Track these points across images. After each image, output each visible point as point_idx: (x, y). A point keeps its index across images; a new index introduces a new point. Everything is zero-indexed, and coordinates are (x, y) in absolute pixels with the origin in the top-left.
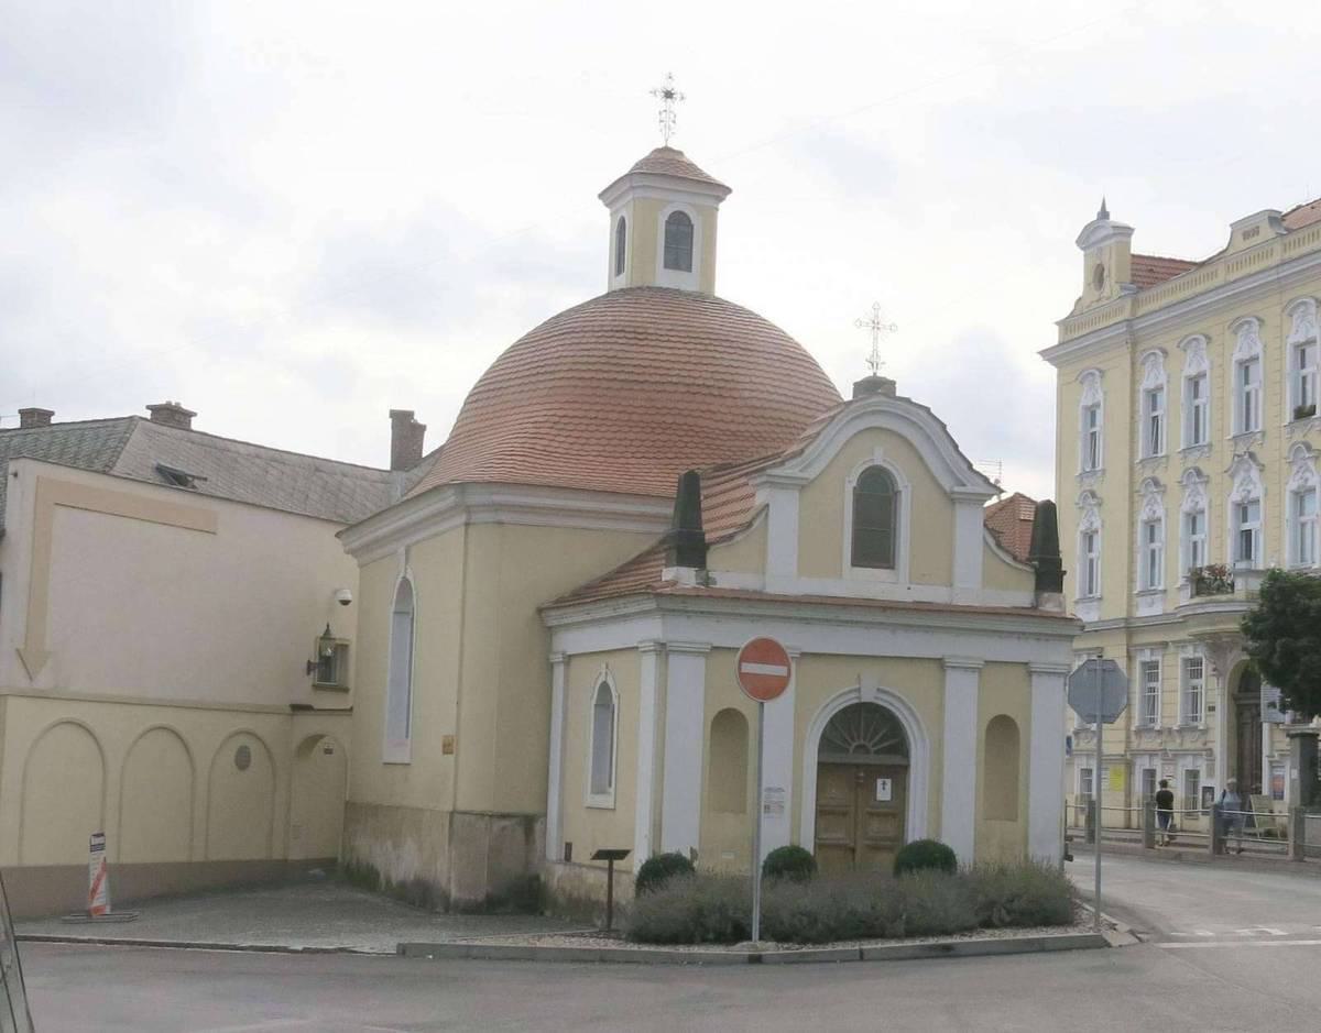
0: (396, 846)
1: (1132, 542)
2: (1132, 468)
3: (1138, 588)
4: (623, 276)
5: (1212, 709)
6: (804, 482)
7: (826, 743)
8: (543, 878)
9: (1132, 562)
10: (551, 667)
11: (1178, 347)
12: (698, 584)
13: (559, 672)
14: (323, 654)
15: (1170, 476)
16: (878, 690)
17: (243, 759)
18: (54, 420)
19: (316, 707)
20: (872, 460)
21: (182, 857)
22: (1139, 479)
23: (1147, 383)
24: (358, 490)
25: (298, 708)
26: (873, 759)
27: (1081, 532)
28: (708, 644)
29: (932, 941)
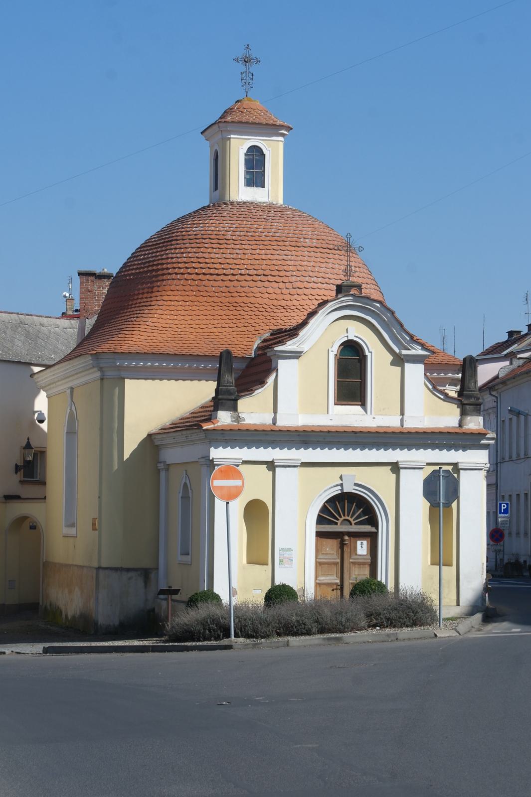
0: (70, 592)
4: (218, 191)
7: (320, 520)
8: (156, 610)
12: (232, 421)
13: (163, 474)
19: (22, 497)
20: (347, 336)
29: (333, 635)
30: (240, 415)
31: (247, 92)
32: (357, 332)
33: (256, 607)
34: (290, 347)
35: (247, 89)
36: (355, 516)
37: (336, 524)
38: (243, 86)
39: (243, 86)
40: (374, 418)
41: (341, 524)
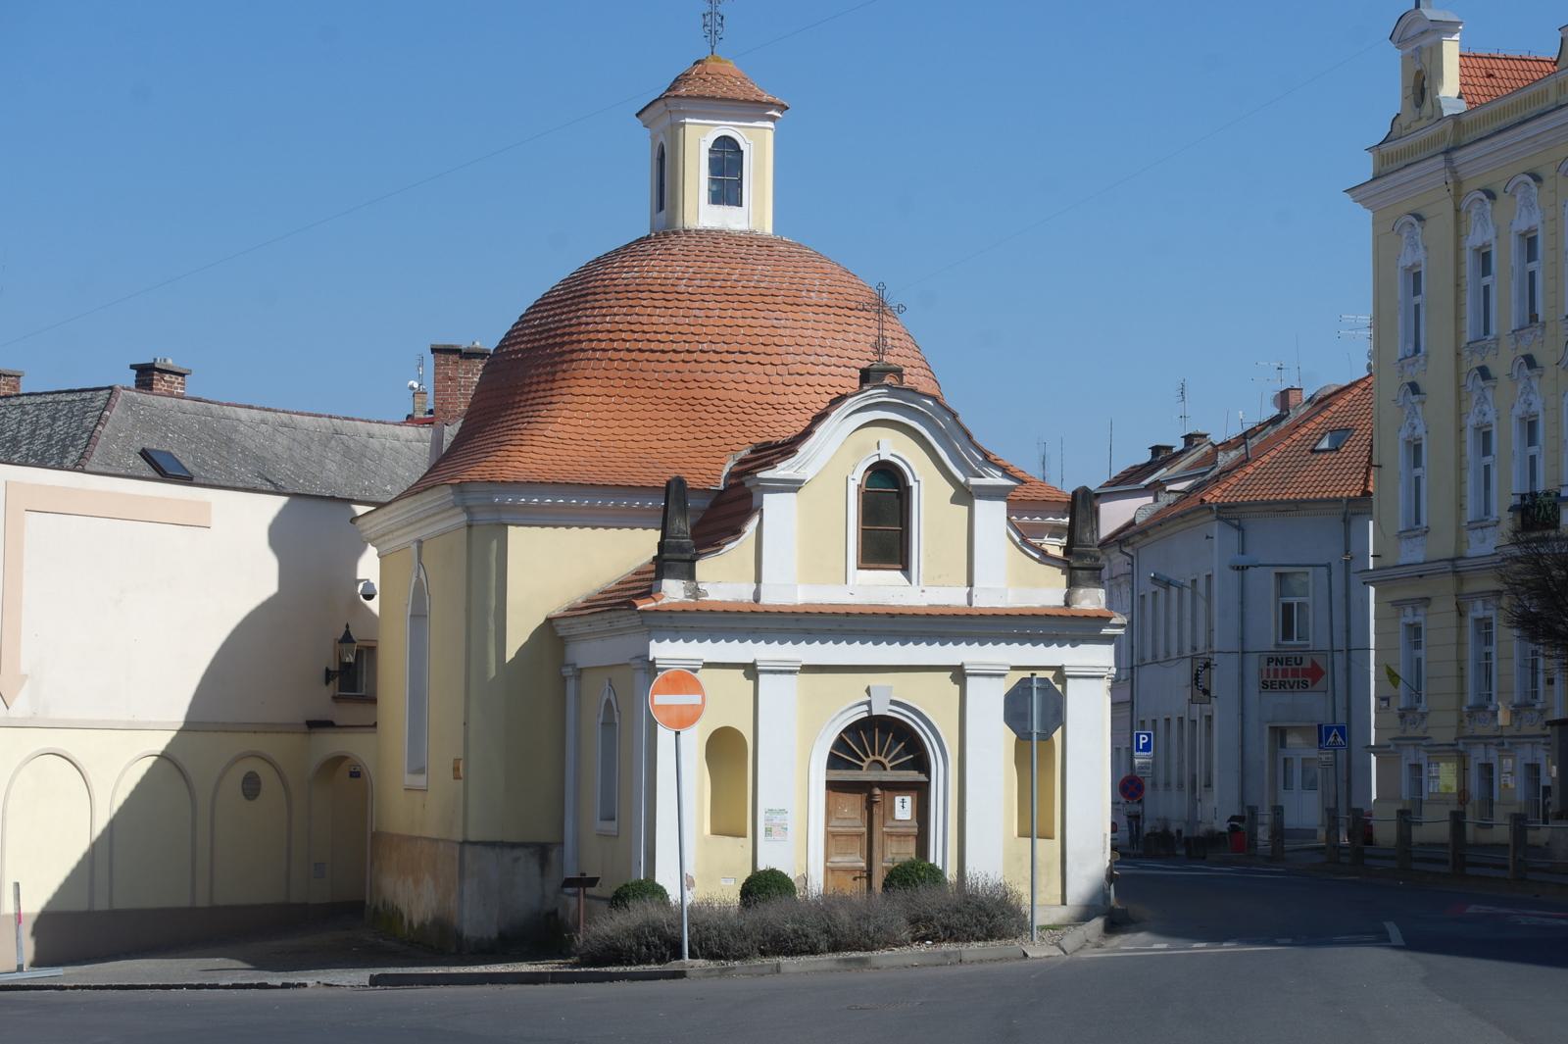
1: (1460, 455)
2: (1458, 354)
3: (1470, 514)
5: (1551, 682)
9: (1460, 482)
10: (565, 679)
11: (1505, 192)
12: (687, 597)
13: (571, 685)
14: (343, 660)
15: (1502, 364)
17: (251, 786)
19: (337, 723)
20: (879, 455)
21: (185, 902)
22: (1465, 368)
23: (1475, 238)
24: (388, 452)
25: (315, 725)
26: (891, 776)
27: (1403, 440)
30: (700, 586)
31: (713, 47)
32: (895, 447)
33: (724, 912)
34: (782, 472)
36: (893, 764)
37: (861, 768)
40: (923, 591)
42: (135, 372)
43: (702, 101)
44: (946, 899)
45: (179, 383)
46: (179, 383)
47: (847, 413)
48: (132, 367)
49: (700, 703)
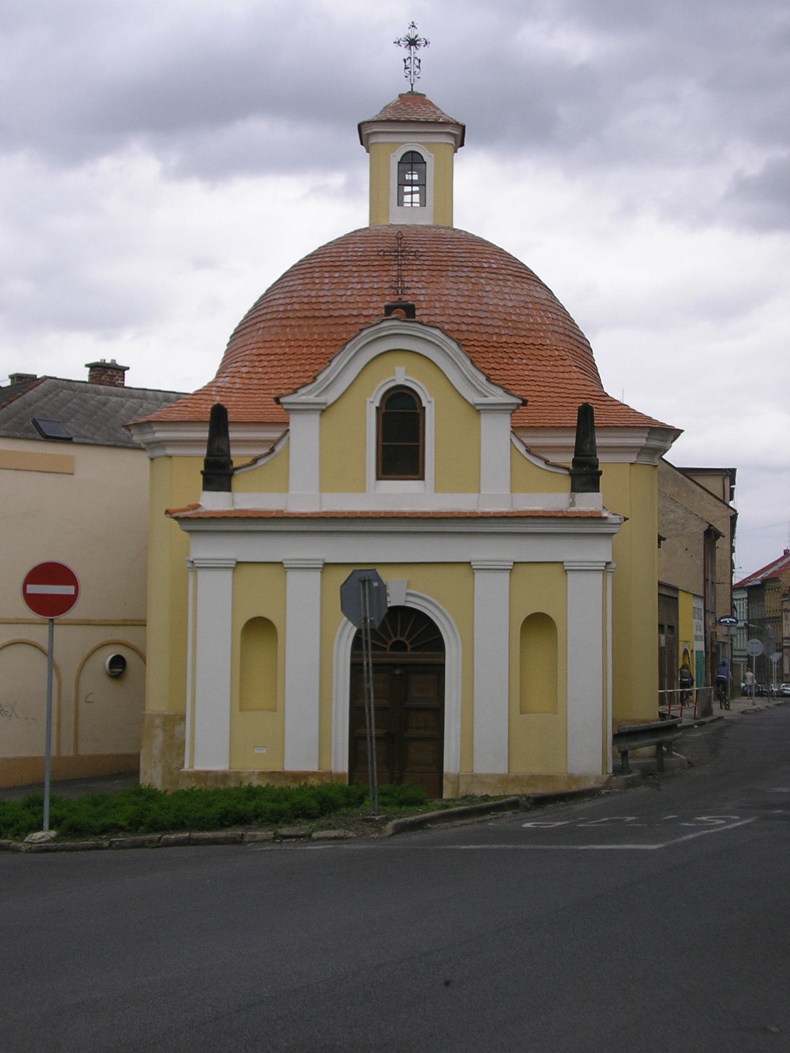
6: (324, 407)
16: (408, 594)
18: (129, 382)
28: (234, 560)
31: (412, 85)
35: (412, 80)
36: (399, 633)
37: (385, 649)
38: (406, 77)
39: (406, 77)
41: (392, 649)
42: (88, 369)
43: (390, 124)
44: (567, 773)
45: (119, 376)
46: (119, 376)
47: (362, 344)
48: (87, 366)
49: (73, 592)
